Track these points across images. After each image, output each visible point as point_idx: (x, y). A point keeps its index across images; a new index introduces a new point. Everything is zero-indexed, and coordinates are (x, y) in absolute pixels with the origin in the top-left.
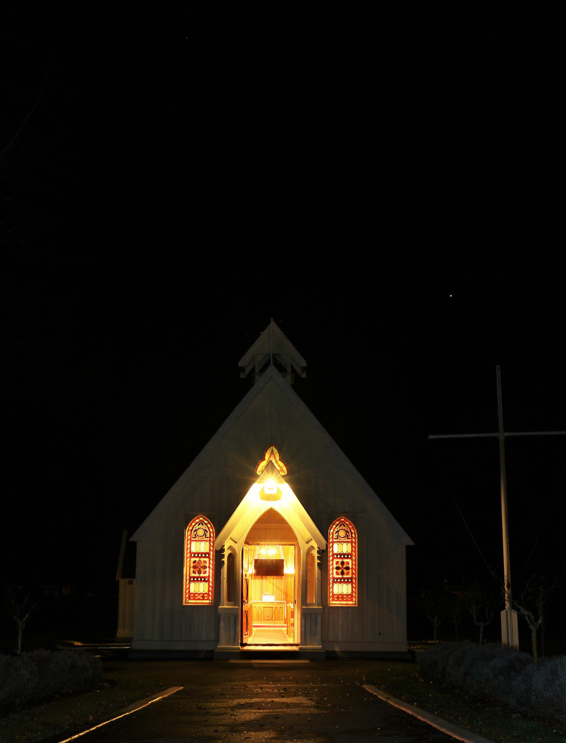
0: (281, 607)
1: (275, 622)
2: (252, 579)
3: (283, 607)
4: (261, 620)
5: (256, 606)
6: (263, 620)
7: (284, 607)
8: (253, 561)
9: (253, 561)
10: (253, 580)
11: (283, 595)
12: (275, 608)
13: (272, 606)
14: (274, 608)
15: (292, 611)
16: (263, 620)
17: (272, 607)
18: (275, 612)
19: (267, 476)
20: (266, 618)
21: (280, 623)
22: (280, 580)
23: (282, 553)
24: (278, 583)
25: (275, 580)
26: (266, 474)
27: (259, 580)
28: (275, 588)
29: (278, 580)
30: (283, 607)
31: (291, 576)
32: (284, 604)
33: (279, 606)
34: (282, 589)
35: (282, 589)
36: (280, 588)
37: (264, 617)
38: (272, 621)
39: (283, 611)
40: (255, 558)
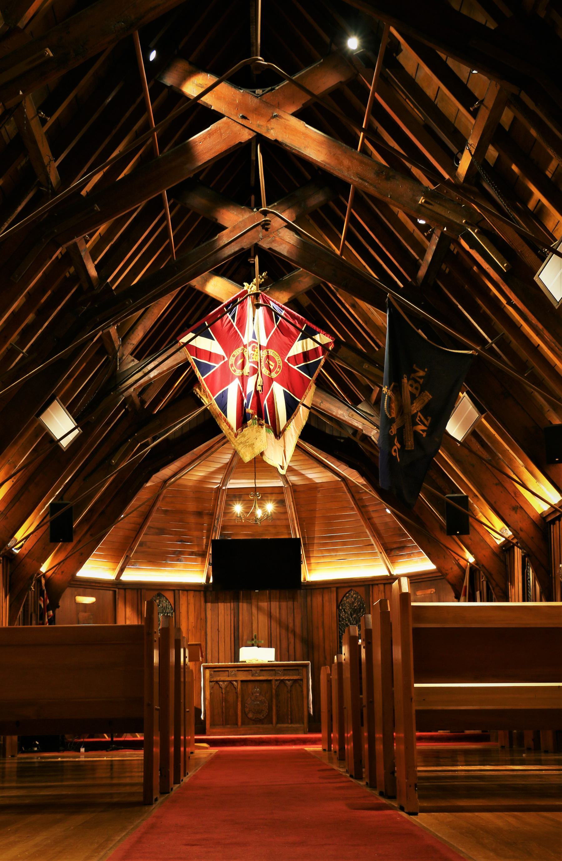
0: (295, 681)
1: (279, 725)
2: (206, 602)
3: (302, 680)
4: (237, 724)
5: (218, 679)
6: (243, 723)
7: (305, 681)
8: (207, 546)
9: (207, 546)
10: (209, 605)
11: (299, 645)
12: (277, 683)
13: (270, 678)
14: (274, 685)
15: (328, 673)
16: (243, 723)
17: (270, 681)
18: (277, 695)
19: (268, 503)
20: (250, 715)
21: (296, 731)
22: (290, 603)
23: (293, 521)
24: (284, 612)
25: (275, 605)
26: (272, 503)
27: (229, 604)
28: (274, 624)
29: (284, 604)
30: (302, 680)
31: (323, 588)
32: (304, 670)
33: (292, 678)
34: (298, 630)
35: (298, 630)
36: (291, 625)
37: (244, 712)
38: (270, 726)
39: (302, 691)
40: (213, 538)
